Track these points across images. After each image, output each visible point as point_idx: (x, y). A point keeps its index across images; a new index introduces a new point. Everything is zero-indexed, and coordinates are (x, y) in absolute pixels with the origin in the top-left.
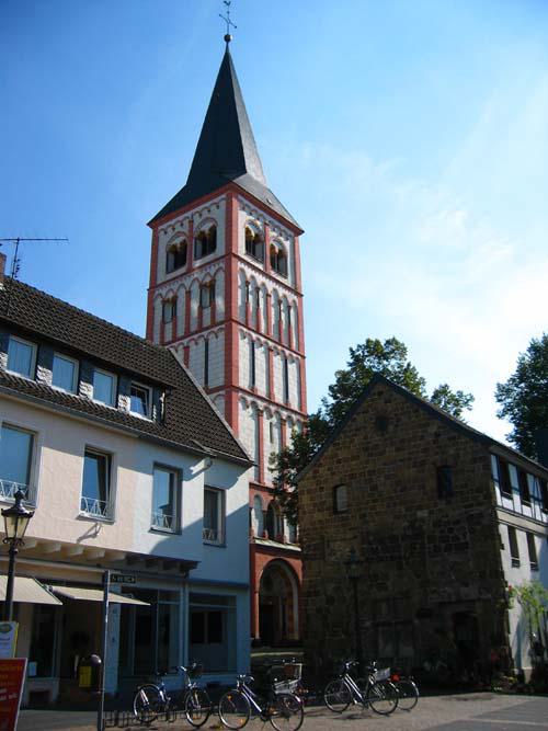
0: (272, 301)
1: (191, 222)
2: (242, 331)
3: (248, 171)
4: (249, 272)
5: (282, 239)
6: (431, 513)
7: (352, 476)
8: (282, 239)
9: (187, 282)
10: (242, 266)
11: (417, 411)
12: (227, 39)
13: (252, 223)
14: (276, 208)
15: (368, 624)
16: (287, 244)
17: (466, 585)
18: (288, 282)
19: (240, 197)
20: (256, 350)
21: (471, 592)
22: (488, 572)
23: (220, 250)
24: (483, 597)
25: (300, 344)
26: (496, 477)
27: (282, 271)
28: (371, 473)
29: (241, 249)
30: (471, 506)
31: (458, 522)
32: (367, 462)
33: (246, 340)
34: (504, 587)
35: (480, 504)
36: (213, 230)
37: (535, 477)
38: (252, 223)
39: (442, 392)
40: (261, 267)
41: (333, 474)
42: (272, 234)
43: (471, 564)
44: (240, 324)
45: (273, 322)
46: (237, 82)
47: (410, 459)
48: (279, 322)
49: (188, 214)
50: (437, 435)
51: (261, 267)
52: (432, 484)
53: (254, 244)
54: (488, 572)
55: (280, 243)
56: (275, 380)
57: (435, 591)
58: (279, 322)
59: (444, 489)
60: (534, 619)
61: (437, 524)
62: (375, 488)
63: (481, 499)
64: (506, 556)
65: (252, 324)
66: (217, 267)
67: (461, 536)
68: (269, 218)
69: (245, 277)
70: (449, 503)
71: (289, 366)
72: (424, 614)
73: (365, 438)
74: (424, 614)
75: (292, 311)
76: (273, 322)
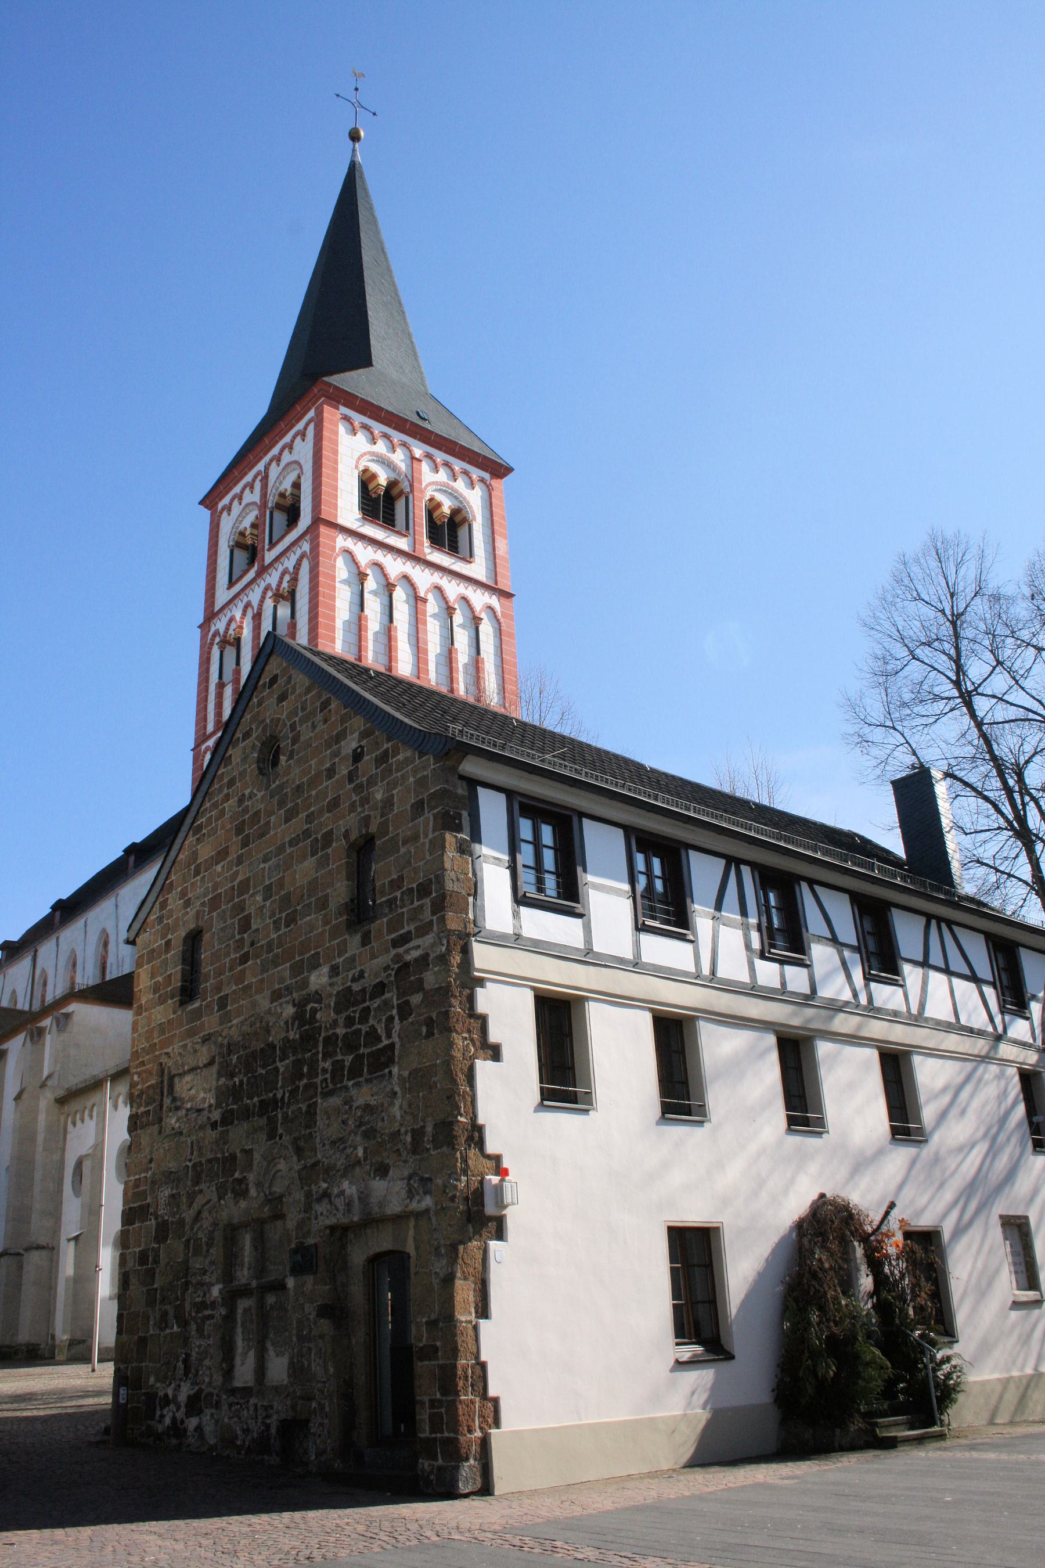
1: (265, 478)
3: (374, 363)
4: (365, 554)
6: (334, 971)
7: (214, 903)
9: (254, 596)
10: (349, 543)
11: (325, 705)
12: (354, 137)
13: (382, 461)
14: (465, 441)
15: (215, 1291)
16: (474, 499)
17: (382, 1171)
18: (478, 569)
21: (390, 1193)
22: (429, 1129)
23: (305, 520)
24: (414, 1206)
26: (774, 910)
28: (244, 887)
29: (347, 509)
30: (405, 939)
31: (380, 988)
32: (240, 861)
34: (454, 1174)
35: (424, 930)
36: (296, 485)
37: (732, 862)
40: (402, 543)
41: (188, 903)
43: (396, 1111)
47: (307, 833)
49: (260, 466)
50: (357, 756)
51: (402, 543)
52: (340, 891)
53: (381, 503)
54: (429, 1129)
55: (453, 494)
56: (938, 906)
57: (326, 1195)
59: (359, 913)
61: (346, 999)
62: (245, 925)
63: (427, 915)
64: (504, 1091)
66: (263, 585)
67: (381, 1030)
70: (366, 941)
72: (304, 1261)
73: (241, 801)
74: (304, 1261)
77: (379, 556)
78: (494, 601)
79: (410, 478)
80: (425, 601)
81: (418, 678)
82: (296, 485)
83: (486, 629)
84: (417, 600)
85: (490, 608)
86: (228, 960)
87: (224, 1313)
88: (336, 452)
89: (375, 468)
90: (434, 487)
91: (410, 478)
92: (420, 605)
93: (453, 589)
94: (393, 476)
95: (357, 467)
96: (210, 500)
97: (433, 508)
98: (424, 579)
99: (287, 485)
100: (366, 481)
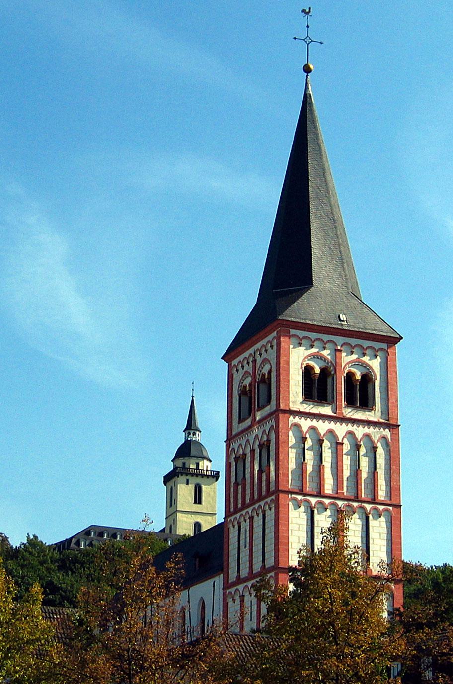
0: (346, 447)
2: (295, 499)
5: (366, 359)
8: (366, 359)
13: (315, 357)
16: (375, 364)
19: (293, 332)
20: (316, 517)
25: (393, 489)
27: (366, 403)
33: (302, 508)
36: (270, 372)
38: (315, 357)
39: (188, 535)
42: (346, 359)
44: (292, 493)
45: (347, 473)
46: (317, 134)
48: (356, 472)
51: (327, 410)
53: (317, 386)
55: (365, 365)
58: (356, 472)
60: (242, 650)
65: (309, 487)
68: (340, 340)
69: (301, 431)
71: (372, 522)
75: (240, 487)
76: (347, 473)
77: (314, 423)
78: (387, 432)
79: (334, 362)
80: (342, 444)
81: (337, 493)
82: (270, 372)
83: (381, 452)
84: (338, 445)
85: (384, 437)
86: (346, 301)
87: (358, 517)
88: (288, 363)
89: (312, 363)
90: (350, 365)
91: (334, 362)
92: (339, 447)
93: (360, 431)
94: (323, 364)
95: (301, 368)
96: (228, 357)
97: (350, 376)
98: (341, 430)
99: (265, 370)
100: (308, 372)
